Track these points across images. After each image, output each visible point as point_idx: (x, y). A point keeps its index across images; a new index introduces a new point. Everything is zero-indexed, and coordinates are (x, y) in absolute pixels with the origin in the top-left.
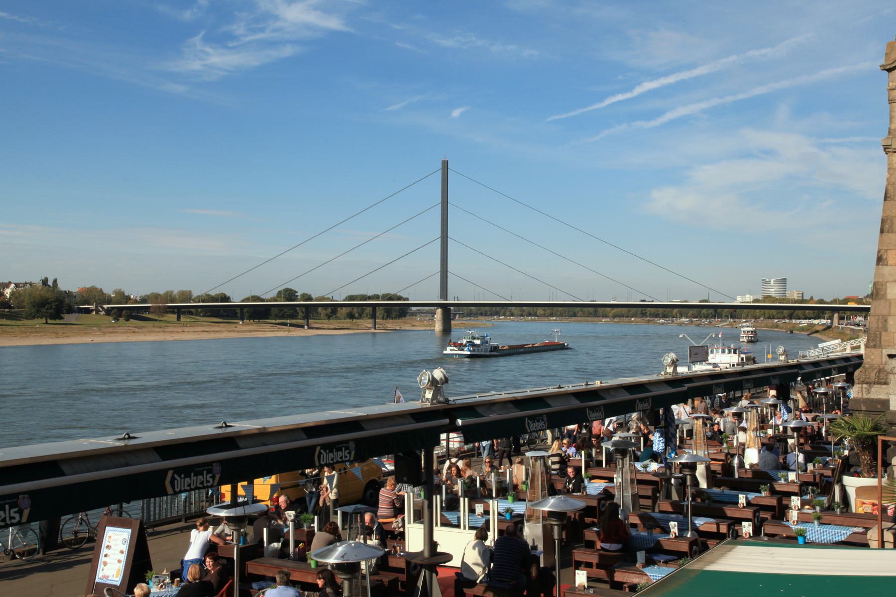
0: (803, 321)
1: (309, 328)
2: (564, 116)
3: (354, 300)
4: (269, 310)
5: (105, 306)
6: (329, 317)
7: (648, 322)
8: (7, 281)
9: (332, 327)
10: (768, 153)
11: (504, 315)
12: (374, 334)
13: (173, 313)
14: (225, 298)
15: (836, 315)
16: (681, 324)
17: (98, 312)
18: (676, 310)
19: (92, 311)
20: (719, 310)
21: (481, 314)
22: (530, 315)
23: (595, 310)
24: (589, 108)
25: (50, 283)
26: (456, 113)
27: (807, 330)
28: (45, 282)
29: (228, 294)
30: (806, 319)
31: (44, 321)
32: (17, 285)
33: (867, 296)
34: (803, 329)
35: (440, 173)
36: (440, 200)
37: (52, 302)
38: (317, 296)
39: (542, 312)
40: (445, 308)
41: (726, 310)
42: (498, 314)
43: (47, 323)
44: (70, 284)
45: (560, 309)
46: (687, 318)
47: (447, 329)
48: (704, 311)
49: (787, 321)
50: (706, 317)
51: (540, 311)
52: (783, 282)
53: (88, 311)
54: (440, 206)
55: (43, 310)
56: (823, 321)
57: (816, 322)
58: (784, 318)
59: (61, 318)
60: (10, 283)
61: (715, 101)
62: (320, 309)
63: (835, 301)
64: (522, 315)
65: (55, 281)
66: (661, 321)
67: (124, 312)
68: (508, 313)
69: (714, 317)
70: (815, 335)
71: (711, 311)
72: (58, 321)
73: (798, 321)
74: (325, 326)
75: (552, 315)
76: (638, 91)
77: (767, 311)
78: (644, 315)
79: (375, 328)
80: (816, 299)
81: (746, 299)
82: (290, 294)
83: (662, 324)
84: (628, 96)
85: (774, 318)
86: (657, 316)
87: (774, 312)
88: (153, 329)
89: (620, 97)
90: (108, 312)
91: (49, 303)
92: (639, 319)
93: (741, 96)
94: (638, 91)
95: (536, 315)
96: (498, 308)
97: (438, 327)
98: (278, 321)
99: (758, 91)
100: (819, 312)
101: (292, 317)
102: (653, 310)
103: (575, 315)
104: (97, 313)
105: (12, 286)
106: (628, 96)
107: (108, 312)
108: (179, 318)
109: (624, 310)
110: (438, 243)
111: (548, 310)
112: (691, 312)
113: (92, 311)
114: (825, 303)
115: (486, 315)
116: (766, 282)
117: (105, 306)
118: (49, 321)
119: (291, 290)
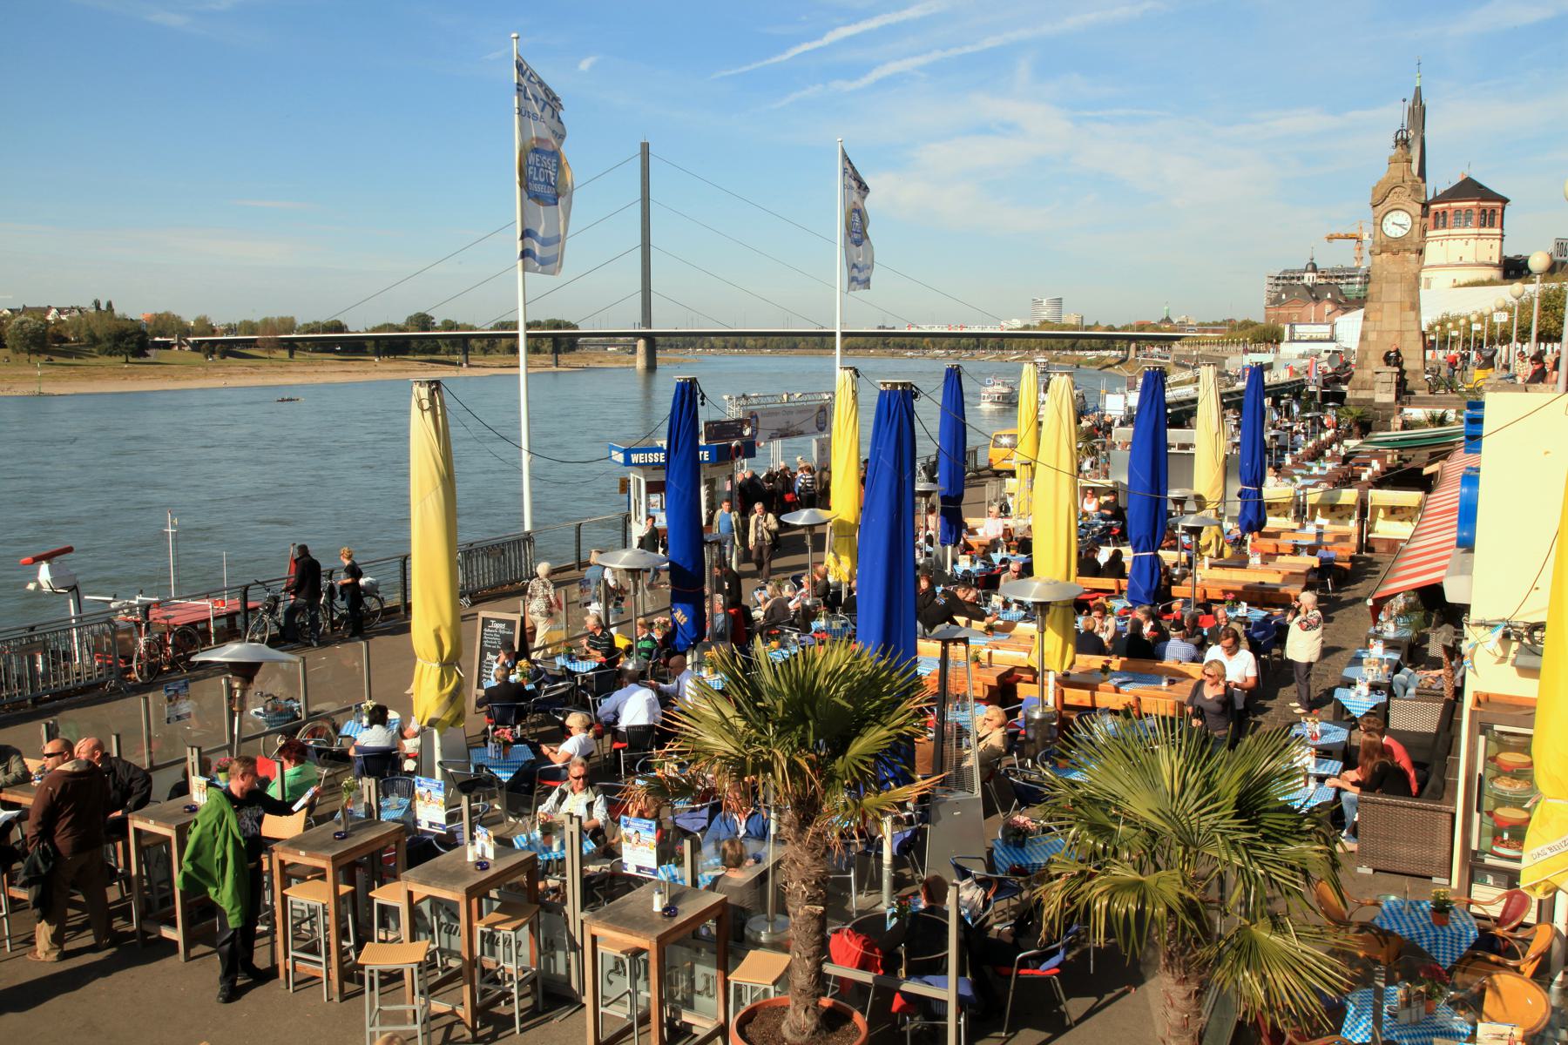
0: (1089, 353)
1: (469, 366)
2: (733, 72)
3: (506, 329)
4: (409, 343)
5: (191, 339)
6: (485, 351)
7: (893, 355)
8: (45, 305)
9: (497, 364)
10: (1009, 128)
11: (702, 346)
12: (555, 373)
13: (284, 348)
14: (339, 327)
15: (1133, 345)
16: (935, 358)
17: (181, 346)
18: (927, 340)
19: (173, 345)
20: (982, 339)
21: (671, 346)
22: (736, 346)
23: (735, 340)
24: (767, 62)
25: (103, 307)
26: (585, 65)
27: (1097, 364)
28: (97, 305)
29: (344, 322)
30: (1091, 350)
31: (123, 359)
32: (60, 311)
33: (1162, 321)
34: (1090, 363)
35: (638, 160)
36: (639, 196)
37: (132, 334)
38: (309, 320)
39: (753, 343)
40: (651, 339)
41: (991, 340)
42: (693, 345)
43: (127, 362)
44: (135, 307)
45: (776, 338)
46: (940, 348)
47: (651, 367)
48: (964, 341)
49: (1069, 353)
50: (967, 349)
51: (750, 341)
52: (1059, 302)
53: (168, 346)
54: (639, 203)
55: (122, 345)
56: (1114, 353)
57: (1105, 353)
58: (1065, 349)
59: (146, 355)
60: (50, 308)
61: (937, 55)
62: (473, 341)
63: (1125, 329)
64: (725, 347)
65: (109, 305)
66: (909, 354)
67: (217, 348)
68: (706, 345)
69: (977, 347)
70: (1108, 370)
71: (973, 340)
72: (142, 360)
73: (1082, 353)
74: (488, 364)
75: (765, 346)
76: (830, 38)
77: (1044, 341)
78: (886, 346)
79: (557, 365)
80: (1104, 324)
81: (1014, 324)
82: (423, 321)
83: (911, 357)
84: (816, 44)
85: (1052, 349)
86: (902, 347)
87: (1053, 341)
88: (272, 369)
89: (806, 47)
90: (196, 347)
91: (129, 336)
92: (881, 351)
93: (968, 49)
94: (830, 38)
95: (744, 347)
96: (693, 338)
97: (640, 362)
98: (417, 357)
99: (990, 42)
100: (1108, 341)
101: (435, 350)
102: (898, 339)
103: (795, 346)
104: (180, 348)
105: (54, 311)
106: (816, 44)
107: (196, 347)
108: (291, 355)
109: (861, 340)
110: (638, 252)
111: (761, 341)
112: (947, 341)
113: (173, 345)
114: (1115, 330)
115: (677, 347)
116: (1037, 303)
117: (191, 339)
118: (131, 359)
119: (425, 315)
